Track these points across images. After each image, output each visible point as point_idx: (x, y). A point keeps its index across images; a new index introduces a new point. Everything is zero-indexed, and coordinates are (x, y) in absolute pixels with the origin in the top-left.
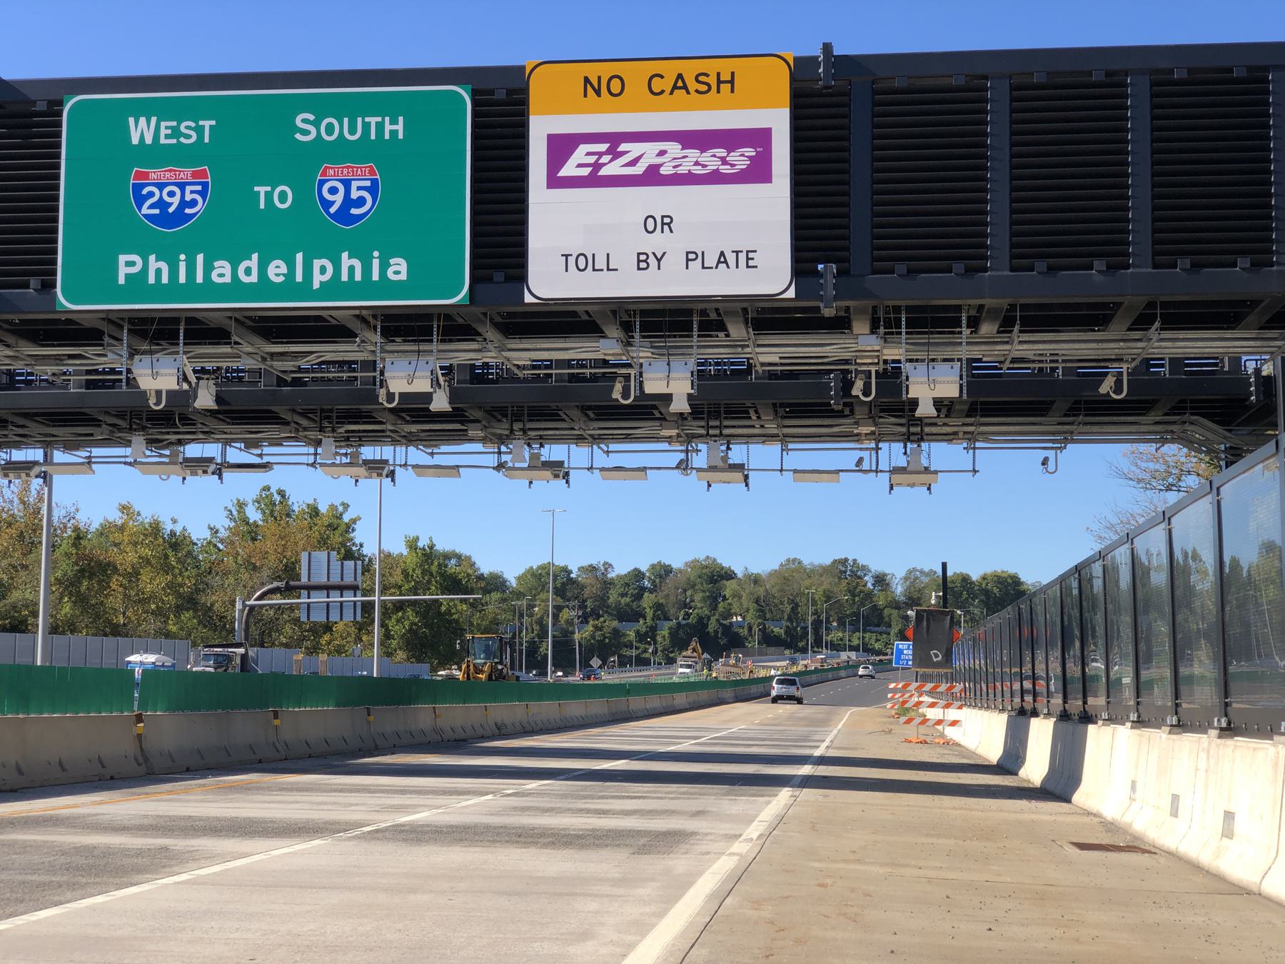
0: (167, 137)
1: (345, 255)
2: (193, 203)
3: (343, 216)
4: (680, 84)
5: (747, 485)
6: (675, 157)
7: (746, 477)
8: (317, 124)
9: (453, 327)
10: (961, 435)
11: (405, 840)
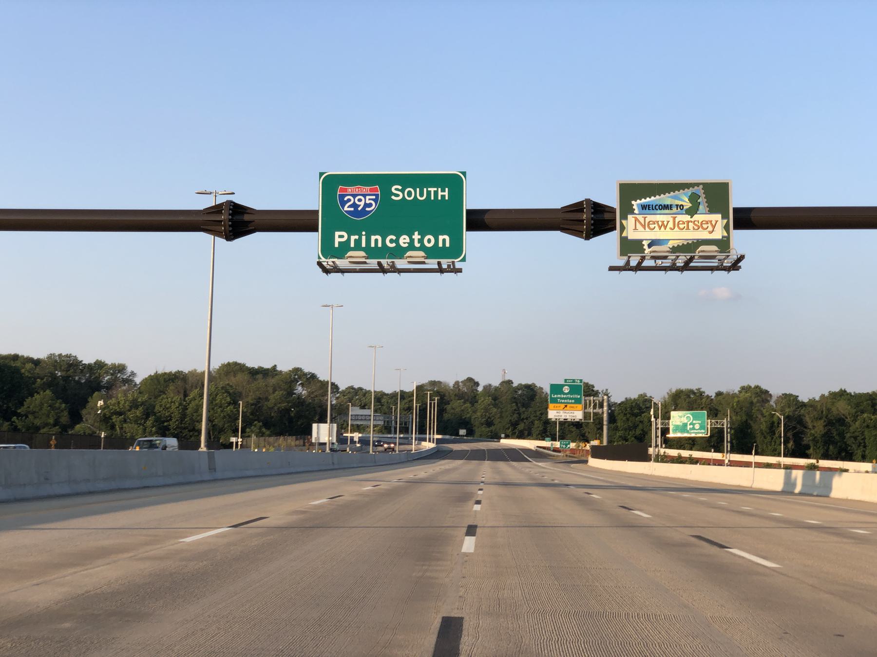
2: (370, 205)
8: (403, 191)
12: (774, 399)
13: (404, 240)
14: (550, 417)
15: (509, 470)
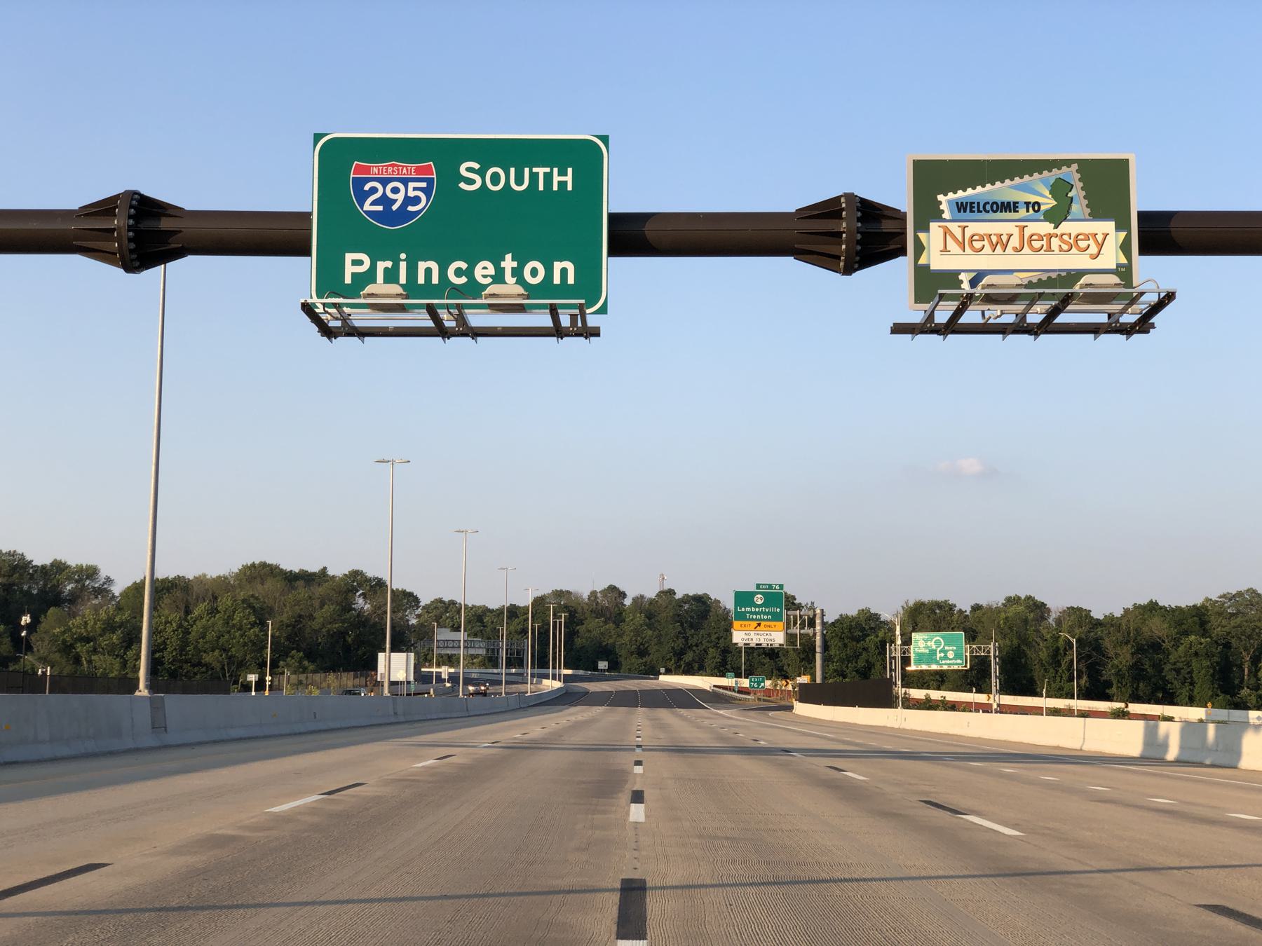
2: (416, 200)
8: (481, 173)
12: (1053, 616)
13: (484, 270)
14: (734, 641)
15: (679, 723)
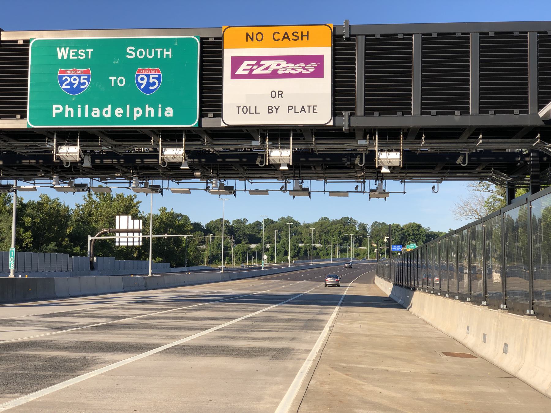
0: (73, 56)
1: (147, 106)
2: (84, 84)
3: (146, 89)
4: (286, 36)
5: (310, 197)
6: (284, 67)
7: (309, 194)
8: (135, 51)
9: (192, 135)
10: (399, 177)
11: (179, 353)
